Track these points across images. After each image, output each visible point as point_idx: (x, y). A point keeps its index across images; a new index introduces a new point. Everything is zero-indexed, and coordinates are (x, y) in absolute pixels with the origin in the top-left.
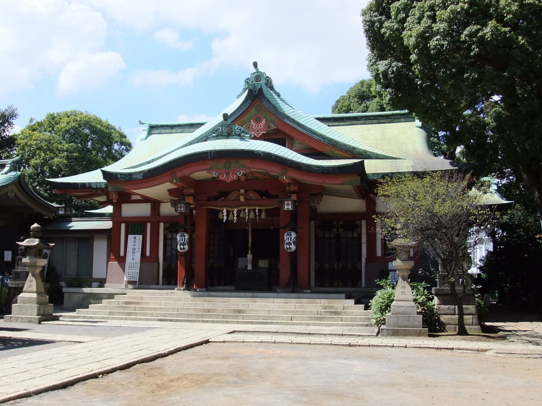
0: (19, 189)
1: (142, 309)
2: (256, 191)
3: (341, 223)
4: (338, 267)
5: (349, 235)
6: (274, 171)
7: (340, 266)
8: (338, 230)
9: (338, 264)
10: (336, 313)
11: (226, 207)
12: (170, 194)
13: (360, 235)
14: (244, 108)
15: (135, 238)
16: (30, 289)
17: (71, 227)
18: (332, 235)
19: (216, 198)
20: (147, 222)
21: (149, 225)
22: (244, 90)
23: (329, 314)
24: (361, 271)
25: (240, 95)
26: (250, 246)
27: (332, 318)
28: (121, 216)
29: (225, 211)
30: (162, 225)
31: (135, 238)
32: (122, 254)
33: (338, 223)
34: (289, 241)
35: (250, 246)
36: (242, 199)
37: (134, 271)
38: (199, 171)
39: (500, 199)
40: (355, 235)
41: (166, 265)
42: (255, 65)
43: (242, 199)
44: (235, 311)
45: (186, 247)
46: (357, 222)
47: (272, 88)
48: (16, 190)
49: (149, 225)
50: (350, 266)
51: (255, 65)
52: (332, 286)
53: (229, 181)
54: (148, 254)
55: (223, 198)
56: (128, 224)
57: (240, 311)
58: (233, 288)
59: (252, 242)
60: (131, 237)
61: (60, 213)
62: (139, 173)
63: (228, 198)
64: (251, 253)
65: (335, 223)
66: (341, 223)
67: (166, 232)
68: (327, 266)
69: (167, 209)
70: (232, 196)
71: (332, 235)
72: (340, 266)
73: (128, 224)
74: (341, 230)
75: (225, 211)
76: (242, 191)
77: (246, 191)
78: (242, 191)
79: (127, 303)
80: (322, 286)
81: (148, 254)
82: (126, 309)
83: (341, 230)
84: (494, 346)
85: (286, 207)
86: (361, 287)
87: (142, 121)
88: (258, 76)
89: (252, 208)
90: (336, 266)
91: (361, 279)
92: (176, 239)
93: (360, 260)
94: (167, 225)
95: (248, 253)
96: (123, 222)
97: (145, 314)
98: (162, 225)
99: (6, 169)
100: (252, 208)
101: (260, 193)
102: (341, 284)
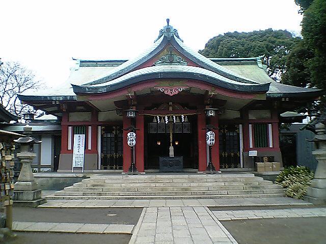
1: (108, 190)
4: (225, 156)
6: (200, 88)
7: (118, 156)
8: (224, 131)
10: (257, 188)
13: (239, 134)
15: (79, 136)
16: (24, 179)
22: (160, 37)
23: (251, 189)
27: (256, 191)
31: (79, 136)
32: (70, 148)
34: (131, 139)
36: (171, 109)
37: (80, 160)
41: (103, 155)
42: (168, 21)
43: (171, 109)
45: (134, 142)
47: (178, 37)
49: (90, 127)
51: (168, 21)
54: (90, 148)
57: (186, 189)
58: (158, 171)
60: (76, 136)
68: (108, 156)
72: (118, 156)
79: (94, 186)
81: (90, 148)
82: (95, 190)
88: (168, 29)
90: (223, 155)
97: (113, 194)
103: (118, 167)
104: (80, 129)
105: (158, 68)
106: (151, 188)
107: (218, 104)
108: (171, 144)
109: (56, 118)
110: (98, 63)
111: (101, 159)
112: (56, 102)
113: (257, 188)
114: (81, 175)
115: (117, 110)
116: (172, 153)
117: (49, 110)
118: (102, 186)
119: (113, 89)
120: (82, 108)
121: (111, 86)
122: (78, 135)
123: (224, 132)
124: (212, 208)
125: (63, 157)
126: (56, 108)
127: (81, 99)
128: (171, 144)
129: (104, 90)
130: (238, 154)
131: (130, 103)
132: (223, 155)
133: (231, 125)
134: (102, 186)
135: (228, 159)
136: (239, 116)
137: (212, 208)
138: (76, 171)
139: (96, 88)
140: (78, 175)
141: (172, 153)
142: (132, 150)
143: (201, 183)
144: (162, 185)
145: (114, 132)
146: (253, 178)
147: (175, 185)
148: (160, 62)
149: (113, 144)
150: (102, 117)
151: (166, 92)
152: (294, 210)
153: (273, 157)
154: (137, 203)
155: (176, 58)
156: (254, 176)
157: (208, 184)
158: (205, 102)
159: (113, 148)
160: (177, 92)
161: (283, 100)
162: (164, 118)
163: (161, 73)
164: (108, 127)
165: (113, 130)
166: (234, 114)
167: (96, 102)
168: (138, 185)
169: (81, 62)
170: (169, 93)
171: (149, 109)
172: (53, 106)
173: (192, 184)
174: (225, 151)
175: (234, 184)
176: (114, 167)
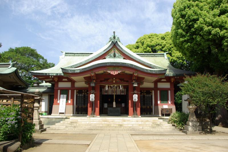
0: (15, 75)
2: (119, 79)
3: (145, 91)
4: (144, 107)
5: (148, 96)
7: (145, 107)
8: (144, 94)
9: (144, 106)
11: (107, 84)
12: (85, 79)
13: (152, 96)
14: (110, 48)
15: (63, 96)
17: (29, 90)
18: (82, 95)
19: (104, 81)
20: (69, 89)
21: (70, 91)
24: (152, 109)
25: (108, 43)
26: (114, 99)
28: (58, 87)
29: (107, 86)
30: (75, 91)
31: (63, 96)
33: (144, 91)
34: (92, 97)
35: (114, 99)
36: (114, 82)
38: (101, 70)
39: (86, 85)
40: (150, 96)
41: (77, 106)
42: (114, 32)
43: (114, 82)
44: (119, 125)
46: (151, 91)
48: (13, 75)
49: (70, 91)
50: (148, 107)
51: (114, 32)
52: (81, 114)
53: (114, 75)
55: (106, 81)
56: (61, 90)
58: (107, 115)
59: (115, 97)
60: (62, 96)
61: (135, 85)
62: (78, 70)
63: (108, 81)
64: (115, 101)
65: (83, 91)
66: (145, 91)
67: (77, 93)
68: (80, 107)
69: (77, 85)
70: (110, 81)
71: (82, 95)
73: (61, 90)
74: (145, 94)
75: (107, 86)
76: (114, 79)
77: (115, 79)
78: (114, 79)
79: (71, 122)
80: (78, 114)
83: (145, 94)
84: (209, 137)
85: (92, 85)
86: (152, 114)
87: (62, 51)
89: (118, 85)
91: (152, 112)
92: (90, 96)
93: (152, 105)
94: (78, 91)
95: (114, 102)
96: (59, 89)
98: (75, 91)
99: (10, 66)
100: (118, 85)
101: (121, 80)
102: (145, 114)
103: (85, 113)
104: (64, 91)
105: (108, 60)
106: (102, 124)
107: (140, 80)
108: (114, 101)
109: (50, 84)
110: (76, 54)
111: (76, 108)
112: (51, 77)
113: (158, 125)
114: (65, 117)
115: (85, 81)
116: (114, 106)
117: (47, 80)
118: (76, 122)
119: (83, 71)
120: (66, 80)
121: (82, 69)
122: (63, 95)
123: (84, 94)
124: (132, 135)
125: (54, 107)
126: (51, 79)
127: (66, 76)
128: (114, 101)
129: (78, 71)
130: (151, 107)
131: (92, 78)
132: (143, 107)
133: (148, 91)
134: (76, 122)
135: (147, 109)
136: (13, 98)
137: (132, 135)
138: (60, 115)
139: (74, 70)
140: (63, 117)
141: (114, 106)
142: (93, 104)
143: (129, 122)
144: (108, 123)
145: (83, 93)
146: (157, 120)
147: (115, 123)
148: (109, 57)
149: (83, 100)
150: (77, 85)
151: (111, 73)
152: (174, 136)
153: (172, 109)
154: (94, 132)
155: (117, 55)
156: (158, 119)
157: (133, 123)
158: (133, 78)
159: (83, 102)
160: (117, 73)
161: (176, 77)
162: (119, 86)
163: (109, 63)
164: (80, 91)
165: (83, 92)
166: (152, 85)
167: (74, 78)
168: (95, 123)
169: (66, 53)
170: (113, 74)
171: (101, 81)
172: (50, 78)
173: (124, 123)
174: (144, 105)
175: (147, 123)
176: (83, 113)
